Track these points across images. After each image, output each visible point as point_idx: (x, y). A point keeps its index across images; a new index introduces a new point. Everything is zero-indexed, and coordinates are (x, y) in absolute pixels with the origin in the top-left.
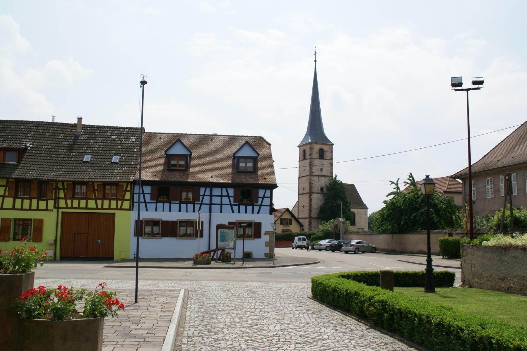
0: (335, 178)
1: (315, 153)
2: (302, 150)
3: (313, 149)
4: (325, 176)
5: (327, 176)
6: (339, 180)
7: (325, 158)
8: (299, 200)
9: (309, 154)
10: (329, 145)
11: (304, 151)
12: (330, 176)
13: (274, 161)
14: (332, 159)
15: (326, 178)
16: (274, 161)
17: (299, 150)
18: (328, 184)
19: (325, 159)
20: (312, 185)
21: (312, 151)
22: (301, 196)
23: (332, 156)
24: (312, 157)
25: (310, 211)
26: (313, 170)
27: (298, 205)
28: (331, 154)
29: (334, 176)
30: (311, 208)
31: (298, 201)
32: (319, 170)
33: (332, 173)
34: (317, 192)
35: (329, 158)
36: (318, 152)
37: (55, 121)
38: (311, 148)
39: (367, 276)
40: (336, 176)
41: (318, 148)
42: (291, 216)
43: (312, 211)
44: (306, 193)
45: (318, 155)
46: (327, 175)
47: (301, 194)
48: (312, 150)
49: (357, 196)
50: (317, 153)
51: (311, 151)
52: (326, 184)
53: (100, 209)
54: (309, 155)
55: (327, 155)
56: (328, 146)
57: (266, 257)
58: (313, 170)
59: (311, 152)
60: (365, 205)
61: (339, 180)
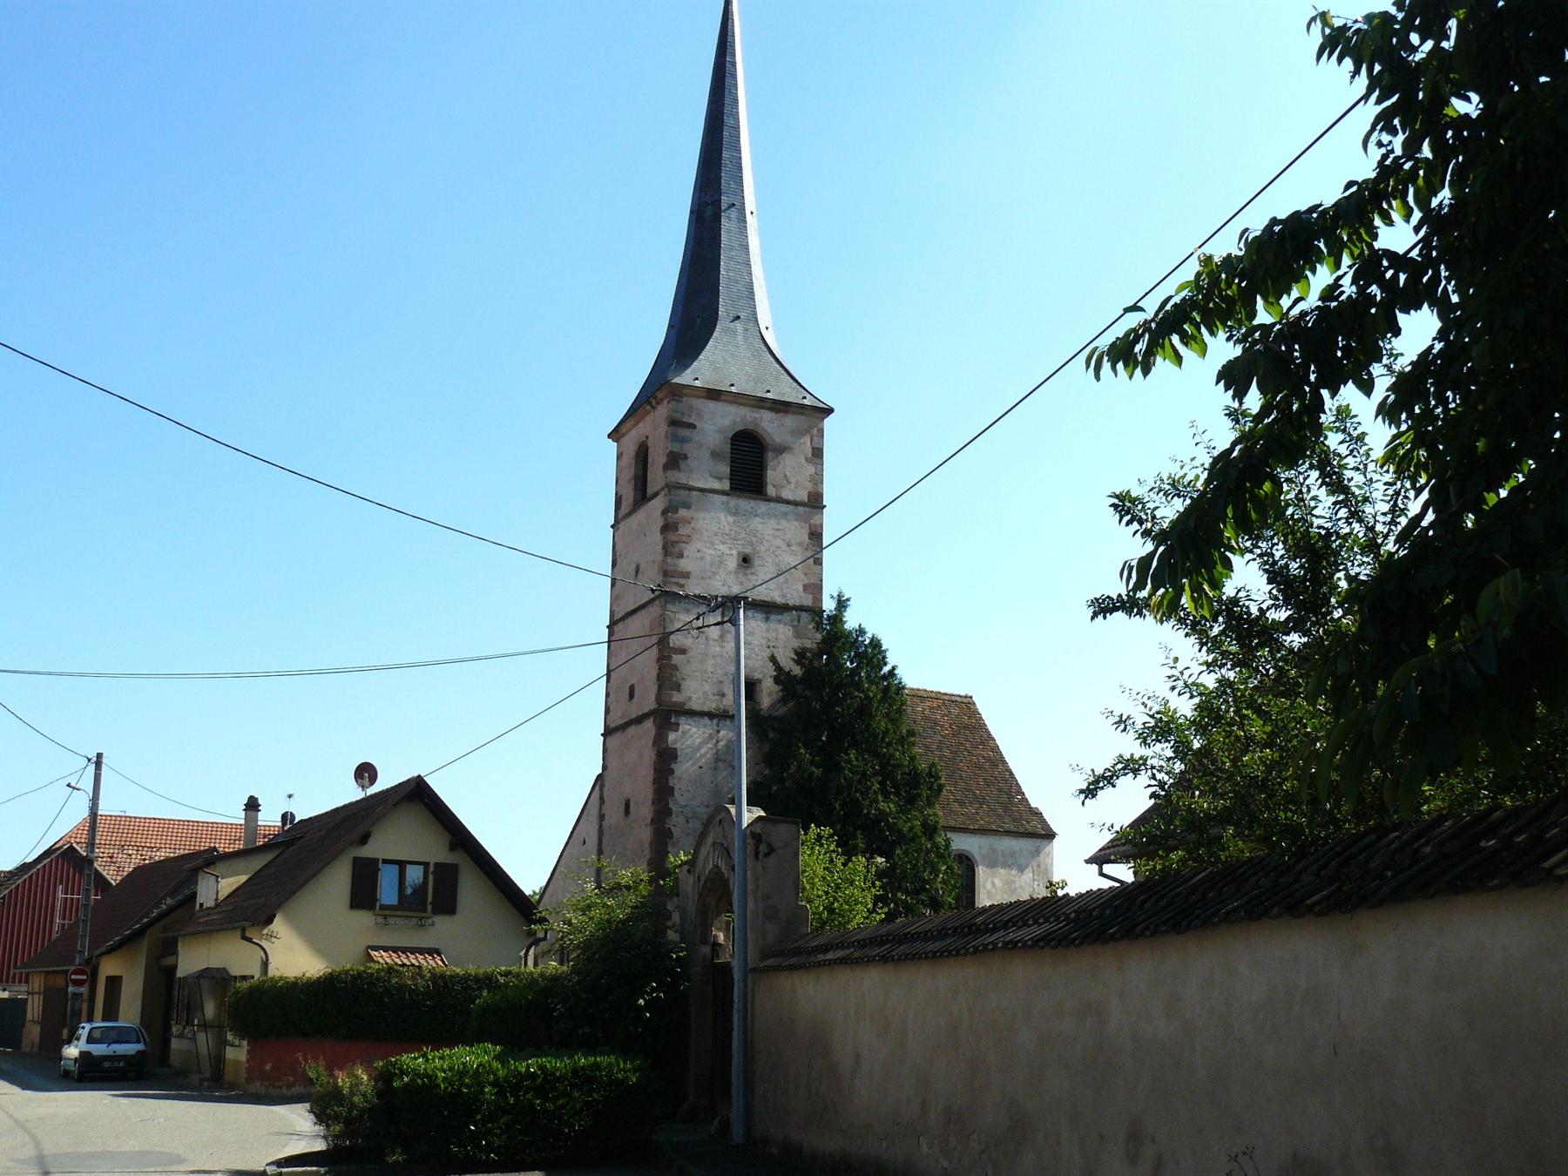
0: (837, 619)
1: (706, 454)
2: (631, 449)
3: (693, 426)
4: (767, 608)
5: (784, 608)
6: (861, 632)
7: (771, 491)
8: (604, 767)
9: (663, 460)
10: (800, 409)
11: (642, 455)
12: (800, 608)
13: (602, 735)
14: (815, 502)
15: (773, 617)
16: (602, 735)
17: (619, 457)
18: (787, 662)
19: (769, 500)
20: (677, 659)
21: (683, 440)
22: (616, 739)
23: (818, 479)
24: (681, 477)
25: (662, 838)
26: (685, 564)
27: (602, 799)
28: (811, 470)
29: (829, 605)
30: (669, 812)
31: (599, 778)
32: (732, 563)
33: (816, 588)
34: (711, 706)
35: (802, 495)
36: (728, 448)
37: (244, 817)
38: (674, 423)
39: (65, 1032)
40: (842, 604)
41: (727, 422)
42: (452, 848)
43: (670, 834)
44: (639, 720)
45: (725, 469)
46: (779, 600)
47: (623, 727)
48: (685, 432)
49: (989, 759)
50: (715, 455)
51: (675, 438)
52: (773, 659)
53: (4, 901)
54: (666, 467)
55: (784, 474)
56: (790, 421)
57: (70, 995)
58: (685, 564)
59: (676, 448)
60: (1037, 814)
61: (861, 632)
